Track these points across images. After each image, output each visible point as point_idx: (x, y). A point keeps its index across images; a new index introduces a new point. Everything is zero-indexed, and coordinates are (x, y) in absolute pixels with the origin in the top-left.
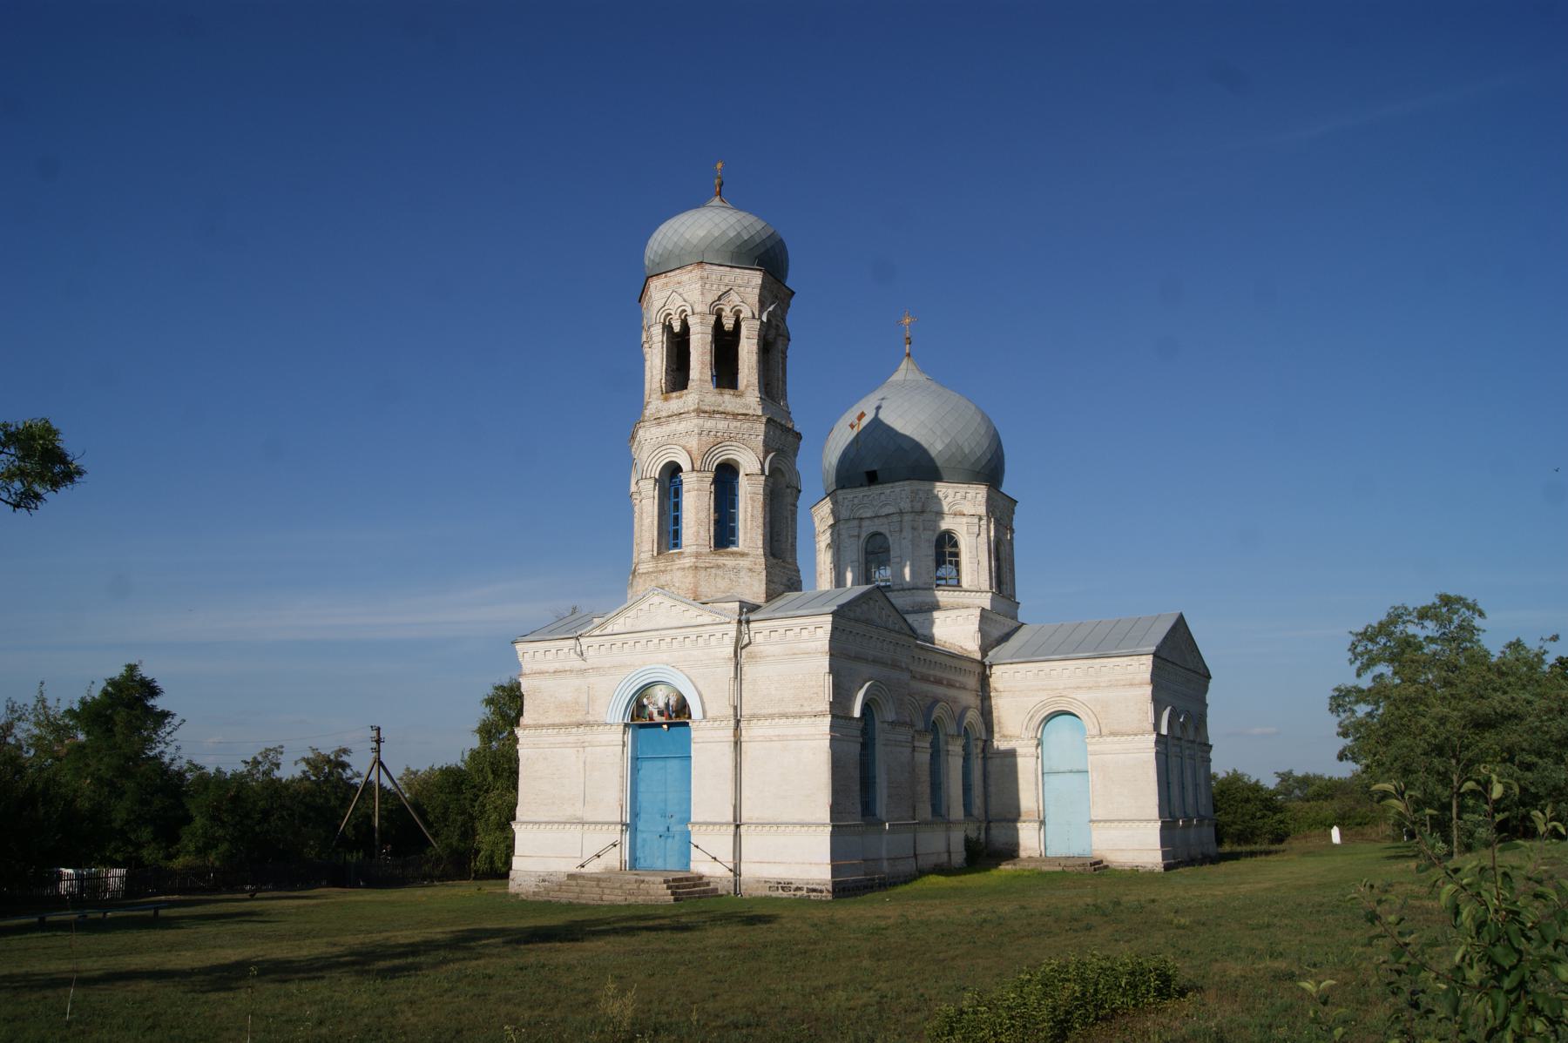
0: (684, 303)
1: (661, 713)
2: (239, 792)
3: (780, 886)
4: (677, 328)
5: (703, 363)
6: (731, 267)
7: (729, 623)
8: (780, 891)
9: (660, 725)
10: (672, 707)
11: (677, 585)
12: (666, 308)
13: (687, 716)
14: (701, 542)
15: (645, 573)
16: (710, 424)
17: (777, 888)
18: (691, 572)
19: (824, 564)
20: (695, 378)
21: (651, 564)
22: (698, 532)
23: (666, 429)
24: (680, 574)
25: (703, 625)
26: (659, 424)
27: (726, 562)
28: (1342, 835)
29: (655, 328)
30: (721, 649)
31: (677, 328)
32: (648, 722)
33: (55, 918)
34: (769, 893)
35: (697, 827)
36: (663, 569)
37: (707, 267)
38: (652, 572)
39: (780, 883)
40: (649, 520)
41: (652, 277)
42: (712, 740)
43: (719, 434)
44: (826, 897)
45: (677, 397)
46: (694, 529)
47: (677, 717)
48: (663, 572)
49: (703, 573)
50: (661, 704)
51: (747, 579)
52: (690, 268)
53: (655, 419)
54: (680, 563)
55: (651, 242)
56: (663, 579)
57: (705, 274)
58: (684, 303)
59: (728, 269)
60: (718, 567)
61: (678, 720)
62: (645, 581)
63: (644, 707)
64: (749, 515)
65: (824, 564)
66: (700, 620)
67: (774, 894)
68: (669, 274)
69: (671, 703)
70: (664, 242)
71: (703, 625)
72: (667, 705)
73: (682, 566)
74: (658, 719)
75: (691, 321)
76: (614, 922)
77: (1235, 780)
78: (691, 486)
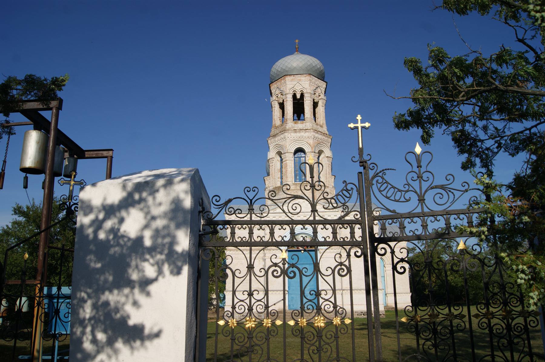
3: (362, 313)
4: (298, 96)
7: (338, 212)
8: (362, 315)
12: (294, 88)
16: (317, 135)
17: (361, 314)
20: (308, 117)
23: (298, 134)
26: (295, 132)
29: (289, 95)
31: (298, 96)
32: (296, 249)
34: (358, 316)
35: (228, 292)
37: (312, 76)
39: (362, 312)
40: (290, 169)
41: (287, 75)
42: (331, 257)
43: (319, 140)
44: (383, 317)
45: (301, 123)
52: (305, 75)
53: (294, 130)
55: (277, 63)
57: (311, 79)
58: (302, 88)
59: (317, 79)
61: (311, 249)
64: (328, 172)
67: (360, 317)
68: (295, 76)
70: (281, 66)
75: (306, 95)
76: (389, 332)
77: (61, 288)
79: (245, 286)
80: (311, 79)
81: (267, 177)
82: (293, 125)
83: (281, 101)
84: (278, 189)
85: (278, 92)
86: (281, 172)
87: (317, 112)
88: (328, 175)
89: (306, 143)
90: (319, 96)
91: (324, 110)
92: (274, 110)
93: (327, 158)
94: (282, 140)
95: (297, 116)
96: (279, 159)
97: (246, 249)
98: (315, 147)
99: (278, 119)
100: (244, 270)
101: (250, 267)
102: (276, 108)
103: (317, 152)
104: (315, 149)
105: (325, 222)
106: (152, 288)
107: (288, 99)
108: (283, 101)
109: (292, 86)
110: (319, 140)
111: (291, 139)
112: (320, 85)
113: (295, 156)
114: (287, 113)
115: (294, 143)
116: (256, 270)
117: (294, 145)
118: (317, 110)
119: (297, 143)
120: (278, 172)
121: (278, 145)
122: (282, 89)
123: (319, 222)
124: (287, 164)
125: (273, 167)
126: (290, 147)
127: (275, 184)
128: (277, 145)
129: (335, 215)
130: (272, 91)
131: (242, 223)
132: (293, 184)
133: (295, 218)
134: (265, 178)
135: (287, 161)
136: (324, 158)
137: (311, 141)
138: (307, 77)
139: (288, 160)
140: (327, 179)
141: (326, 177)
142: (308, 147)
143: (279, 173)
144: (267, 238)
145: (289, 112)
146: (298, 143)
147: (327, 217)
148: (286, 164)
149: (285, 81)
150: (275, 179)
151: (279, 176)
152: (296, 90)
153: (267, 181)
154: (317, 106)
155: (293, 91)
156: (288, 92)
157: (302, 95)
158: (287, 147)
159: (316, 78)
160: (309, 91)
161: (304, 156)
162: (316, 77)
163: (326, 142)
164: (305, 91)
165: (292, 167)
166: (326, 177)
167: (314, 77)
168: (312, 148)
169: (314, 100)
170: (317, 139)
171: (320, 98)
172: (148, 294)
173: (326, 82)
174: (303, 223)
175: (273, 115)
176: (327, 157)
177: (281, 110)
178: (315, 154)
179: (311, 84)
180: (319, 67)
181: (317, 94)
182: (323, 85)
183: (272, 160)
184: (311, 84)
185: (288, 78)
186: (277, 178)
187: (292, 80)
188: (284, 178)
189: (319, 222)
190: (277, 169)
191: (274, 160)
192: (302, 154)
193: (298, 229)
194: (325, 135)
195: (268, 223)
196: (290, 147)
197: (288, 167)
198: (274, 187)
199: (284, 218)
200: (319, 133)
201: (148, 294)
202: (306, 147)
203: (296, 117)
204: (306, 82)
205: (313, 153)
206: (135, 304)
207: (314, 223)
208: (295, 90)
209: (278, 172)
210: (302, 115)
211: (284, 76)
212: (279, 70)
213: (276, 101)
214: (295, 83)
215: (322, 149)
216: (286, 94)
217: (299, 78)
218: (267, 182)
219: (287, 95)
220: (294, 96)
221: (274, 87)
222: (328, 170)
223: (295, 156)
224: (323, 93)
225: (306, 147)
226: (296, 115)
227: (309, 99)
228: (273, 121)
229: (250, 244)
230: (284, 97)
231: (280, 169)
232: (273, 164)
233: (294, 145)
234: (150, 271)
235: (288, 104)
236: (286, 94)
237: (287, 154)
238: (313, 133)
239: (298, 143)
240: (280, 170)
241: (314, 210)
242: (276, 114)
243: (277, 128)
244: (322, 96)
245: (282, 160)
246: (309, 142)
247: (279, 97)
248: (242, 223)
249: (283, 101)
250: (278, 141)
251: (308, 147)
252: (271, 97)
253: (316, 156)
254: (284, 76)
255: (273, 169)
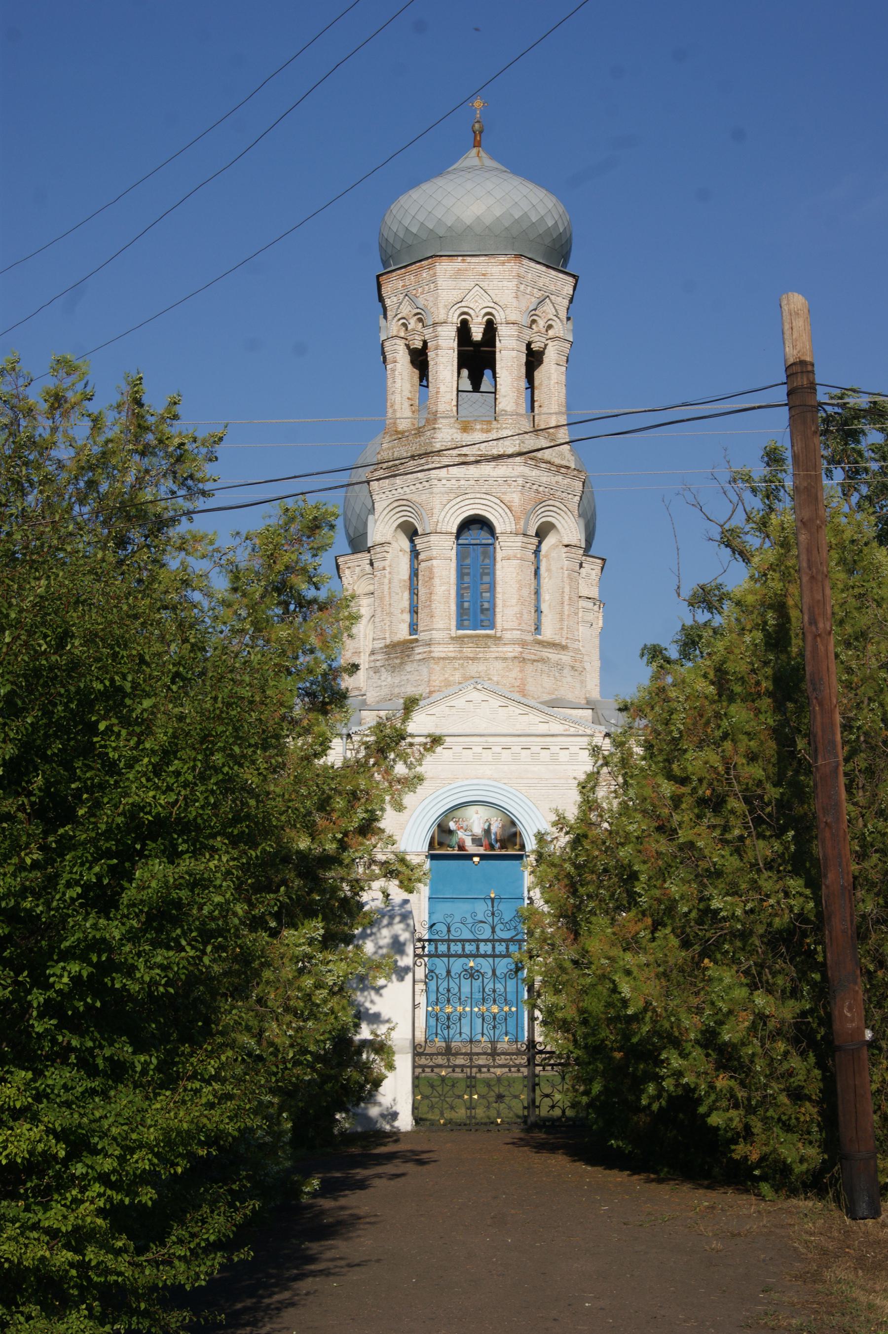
0: (492, 305)
1: (477, 841)
2: (802, 909)
4: (477, 333)
5: (518, 390)
6: (548, 267)
9: (470, 857)
10: (496, 834)
11: (495, 679)
12: (463, 304)
13: (517, 847)
14: (524, 626)
15: (443, 658)
18: (517, 664)
19: (365, 637)
20: (508, 409)
21: (451, 648)
22: (521, 614)
24: (499, 665)
25: (553, 735)
27: (550, 656)
28: (864, 1035)
30: (575, 767)
31: (477, 333)
33: (526, 1034)
36: (471, 655)
37: (525, 262)
38: (454, 658)
40: (443, 588)
43: (541, 489)
46: (516, 609)
47: (502, 848)
48: (473, 659)
49: (529, 668)
50: (478, 830)
51: (569, 679)
54: (495, 650)
56: (473, 669)
58: (492, 305)
59: (544, 269)
60: (542, 660)
61: (503, 852)
62: (443, 669)
63: (451, 832)
64: (567, 597)
65: (365, 637)
66: (543, 728)
68: (469, 259)
69: (494, 829)
71: (553, 735)
72: (487, 832)
73: (502, 655)
74: (471, 848)
78: (510, 552)
79: (445, 984)
80: (522, 271)
81: (347, 558)
82: (455, 436)
83: (418, 345)
84: (402, 652)
85: (406, 309)
86: (414, 591)
87: (541, 384)
88: (566, 608)
89: (498, 502)
90: (550, 327)
91: (564, 377)
92: (393, 370)
93: (566, 549)
94: (418, 486)
95: (470, 377)
96: (406, 544)
97: (445, 959)
98: (528, 514)
99: (406, 404)
100: (444, 974)
101: (449, 972)
102: (398, 366)
103: (532, 531)
104: (527, 523)
105: (501, 940)
106: (383, 991)
107: (441, 342)
108: (425, 343)
109: (456, 295)
110: (541, 489)
111: (448, 484)
112: (552, 288)
113: (460, 542)
114: (438, 392)
115: (458, 500)
116: (453, 974)
117: (457, 507)
118: (538, 374)
119: (467, 502)
120: (403, 592)
121: (404, 502)
122: (421, 302)
123: (497, 941)
124: (435, 570)
125: (386, 572)
126: (443, 513)
127: (391, 633)
128: (403, 503)
129: (506, 935)
130: (388, 302)
131: (443, 941)
132: (452, 638)
133: (480, 937)
134: (340, 560)
135: (434, 562)
136: (555, 546)
137: (515, 498)
138: (508, 266)
139: (435, 558)
140: (562, 620)
141: (561, 613)
142: (503, 514)
143: (406, 595)
144: (460, 952)
145: (443, 389)
146: (472, 501)
147: (558, 751)
148: (430, 569)
149: (435, 275)
150: (390, 614)
151: (406, 604)
152: (471, 312)
153: (347, 572)
154: (541, 362)
155: (458, 312)
156: (442, 317)
157: (490, 328)
158: (436, 511)
159: (538, 266)
160: (513, 317)
161: (490, 541)
162: (539, 263)
163: (564, 495)
164: (499, 317)
165: (448, 583)
166: (561, 613)
167: (532, 264)
168: (517, 519)
169: (529, 345)
170: (535, 487)
171: (551, 333)
172: (381, 995)
173: (574, 276)
174: (486, 941)
175: (390, 392)
176: (567, 546)
177: (417, 372)
178: (525, 540)
179: (522, 287)
180: (550, 223)
181: (541, 323)
182: (564, 285)
183: (383, 549)
184: (522, 287)
185: (444, 268)
186: (397, 612)
187: (458, 275)
188: (422, 614)
189: (497, 941)
190: (400, 581)
191: (390, 550)
192: (483, 537)
193: (482, 945)
194: (563, 470)
195: (460, 941)
196: (443, 513)
197: (437, 581)
198: (388, 642)
199: (471, 937)
200: (543, 465)
201: (381, 995)
202: (496, 514)
203: (467, 385)
204: (505, 283)
205: (520, 538)
206: (372, 1002)
207: (493, 941)
208: (466, 310)
209: (403, 592)
210: (488, 373)
211: (431, 257)
212: (414, 230)
213: (399, 341)
214: (470, 284)
215: (549, 519)
216: (435, 324)
217: (481, 269)
218: (347, 574)
219: (439, 329)
220: (464, 330)
221: (393, 288)
222: (567, 590)
223: (460, 542)
224: (563, 314)
225: (496, 514)
226: (465, 372)
227: (513, 343)
228: (390, 411)
229: (449, 956)
230: (428, 333)
231: (410, 579)
232: (387, 563)
233: (457, 507)
234: (381, 982)
235: (440, 359)
236: (435, 324)
237: (433, 538)
238: (522, 468)
239: (472, 501)
240: (408, 584)
241: (493, 932)
242: (398, 385)
243: (400, 435)
244: (560, 329)
245: (415, 554)
246: (506, 498)
247: (410, 327)
248: (443, 941)
249: (425, 343)
250: (406, 489)
251: (503, 514)
252: (382, 321)
253: (530, 546)
254: (431, 257)
255: (386, 581)
